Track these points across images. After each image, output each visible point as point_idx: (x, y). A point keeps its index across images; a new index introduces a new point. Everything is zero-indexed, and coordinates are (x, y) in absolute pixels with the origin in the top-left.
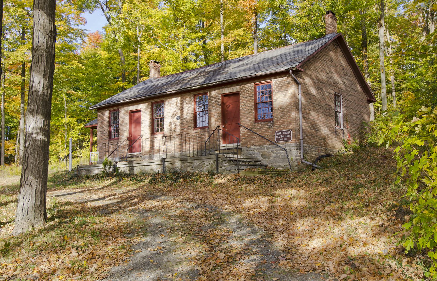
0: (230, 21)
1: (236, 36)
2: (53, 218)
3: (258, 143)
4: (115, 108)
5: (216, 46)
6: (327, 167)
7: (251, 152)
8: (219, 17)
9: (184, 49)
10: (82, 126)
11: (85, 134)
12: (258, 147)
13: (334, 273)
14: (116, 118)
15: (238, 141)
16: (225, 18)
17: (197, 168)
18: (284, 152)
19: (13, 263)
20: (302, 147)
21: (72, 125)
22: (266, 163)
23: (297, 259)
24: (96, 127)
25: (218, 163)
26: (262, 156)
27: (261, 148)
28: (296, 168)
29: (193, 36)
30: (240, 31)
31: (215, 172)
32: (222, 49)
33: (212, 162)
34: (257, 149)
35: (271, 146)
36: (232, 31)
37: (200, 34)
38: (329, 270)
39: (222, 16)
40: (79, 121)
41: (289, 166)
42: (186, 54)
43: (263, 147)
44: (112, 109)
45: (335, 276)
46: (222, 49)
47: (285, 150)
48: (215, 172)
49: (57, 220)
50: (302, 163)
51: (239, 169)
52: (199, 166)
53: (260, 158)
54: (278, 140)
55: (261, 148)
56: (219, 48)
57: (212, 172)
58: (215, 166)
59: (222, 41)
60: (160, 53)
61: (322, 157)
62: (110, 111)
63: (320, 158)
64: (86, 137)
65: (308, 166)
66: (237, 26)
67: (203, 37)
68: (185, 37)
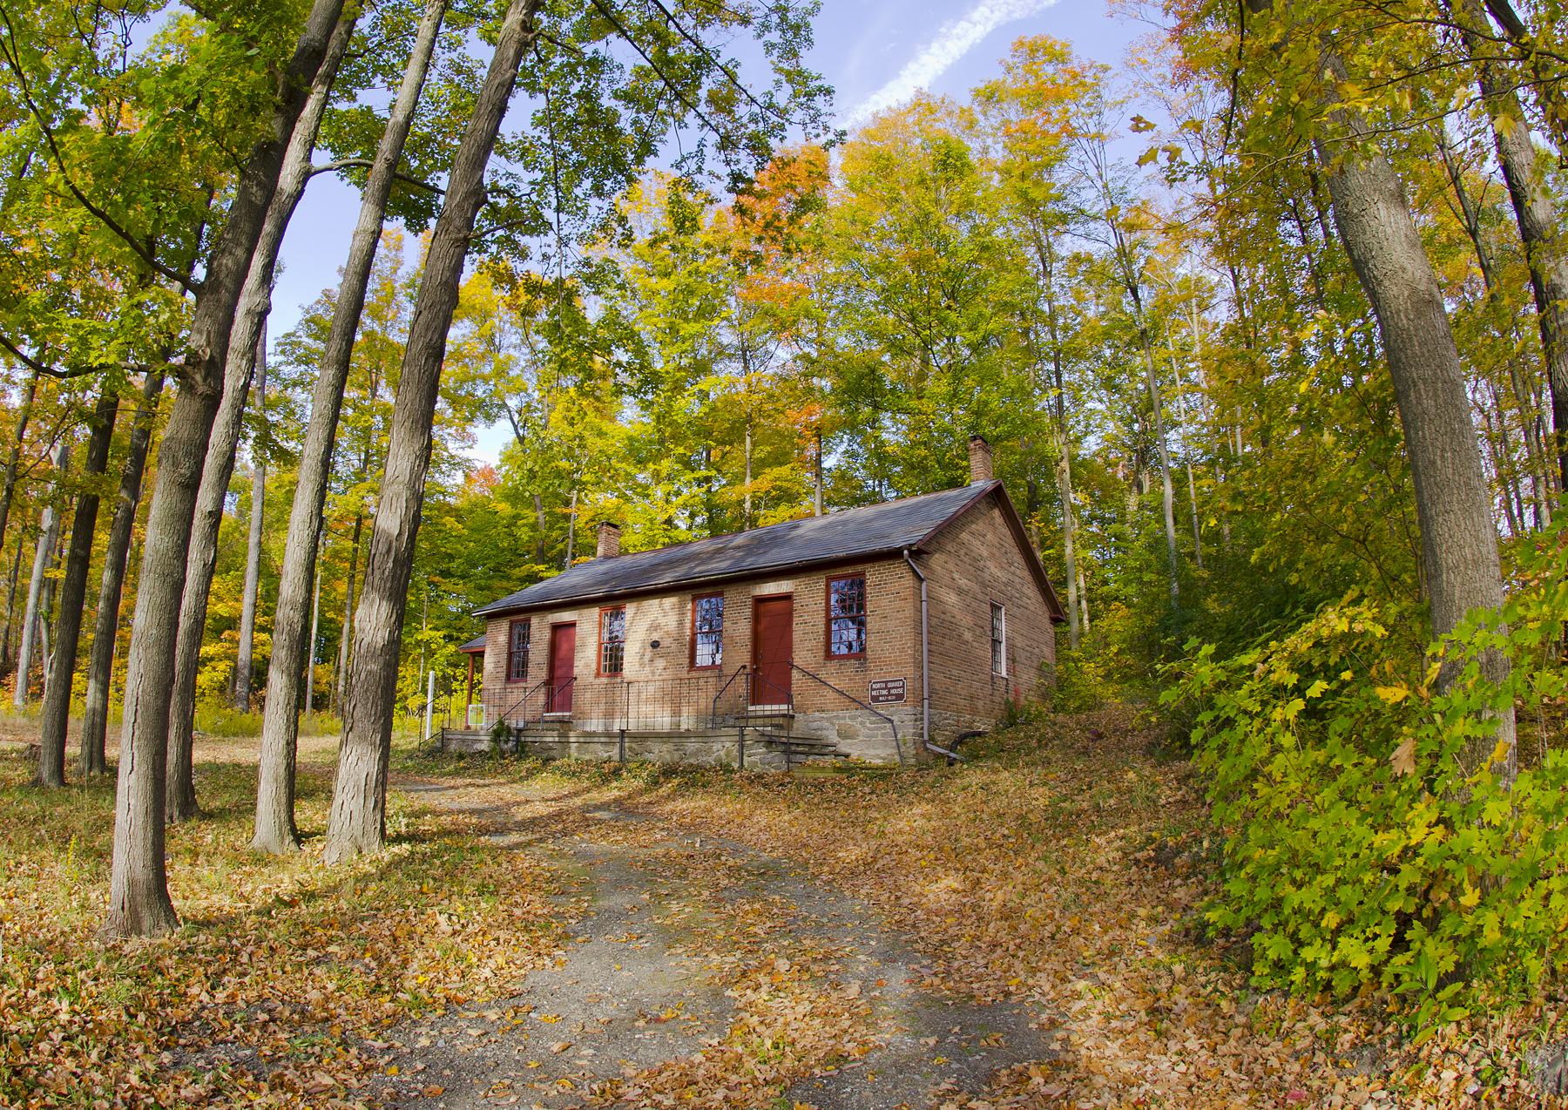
0: (763, 451)
1: (776, 479)
2: (399, 839)
3: (830, 706)
4: (522, 617)
5: (734, 498)
6: (977, 757)
7: (815, 725)
8: (744, 441)
9: (667, 501)
10: (452, 648)
11: (456, 666)
12: (831, 714)
13: (1053, 1000)
14: (525, 637)
15: (788, 699)
16: (754, 444)
17: (696, 754)
18: (889, 725)
19: (324, 927)
20: (926, 717)
21: (434, 646)
22: (847, 750)
23: (959, 970)
24: (481, 654)
25: (742, 747)
26: (839, 735)
27: (837, 717)
28: (912, 761)
29: (689, 476)
30: (784, 471)
31: (736, 765)
32: (747, 505)
33: (728, 744)
34: (828, 719)
35: (859, 712)
36: (767, 470)
37: (703, 473)
38: (1043, 994)
39: (748, 440)
40: (449, 638)
41: (897, 758)
42: (671, 511)
43: (841, 713)
44: (515, 618)
45: (1058, 1007)
46: (747, 505)
47: (891, 721)
48: (736, 765)
49: (406, 846)
50: (926, 749)
51: (789, 761)
52: (698, 750)
53: (833, 737)
54: (875, 699)
55: (837, 717)
56: (741, 503)
57: (729, 765)
58: (735, 753)
59: (748, 488)
60: (618, 508)
61: (966, 736)
62: (512, 623)
63: (961, 740)
64: (459, 672)
65: (939, 756)
66: (778, 459)
67: (708, 479)
68: (670, 478)
